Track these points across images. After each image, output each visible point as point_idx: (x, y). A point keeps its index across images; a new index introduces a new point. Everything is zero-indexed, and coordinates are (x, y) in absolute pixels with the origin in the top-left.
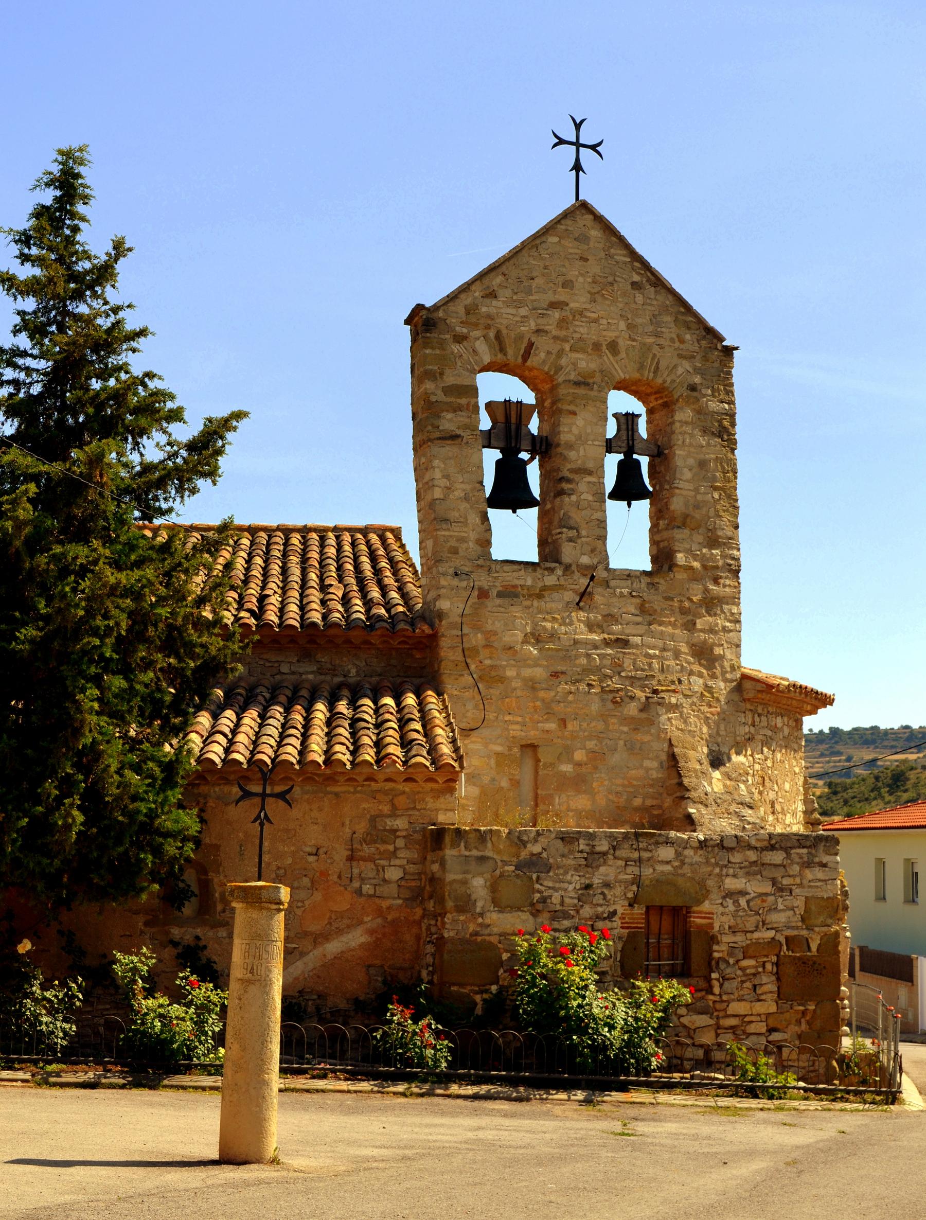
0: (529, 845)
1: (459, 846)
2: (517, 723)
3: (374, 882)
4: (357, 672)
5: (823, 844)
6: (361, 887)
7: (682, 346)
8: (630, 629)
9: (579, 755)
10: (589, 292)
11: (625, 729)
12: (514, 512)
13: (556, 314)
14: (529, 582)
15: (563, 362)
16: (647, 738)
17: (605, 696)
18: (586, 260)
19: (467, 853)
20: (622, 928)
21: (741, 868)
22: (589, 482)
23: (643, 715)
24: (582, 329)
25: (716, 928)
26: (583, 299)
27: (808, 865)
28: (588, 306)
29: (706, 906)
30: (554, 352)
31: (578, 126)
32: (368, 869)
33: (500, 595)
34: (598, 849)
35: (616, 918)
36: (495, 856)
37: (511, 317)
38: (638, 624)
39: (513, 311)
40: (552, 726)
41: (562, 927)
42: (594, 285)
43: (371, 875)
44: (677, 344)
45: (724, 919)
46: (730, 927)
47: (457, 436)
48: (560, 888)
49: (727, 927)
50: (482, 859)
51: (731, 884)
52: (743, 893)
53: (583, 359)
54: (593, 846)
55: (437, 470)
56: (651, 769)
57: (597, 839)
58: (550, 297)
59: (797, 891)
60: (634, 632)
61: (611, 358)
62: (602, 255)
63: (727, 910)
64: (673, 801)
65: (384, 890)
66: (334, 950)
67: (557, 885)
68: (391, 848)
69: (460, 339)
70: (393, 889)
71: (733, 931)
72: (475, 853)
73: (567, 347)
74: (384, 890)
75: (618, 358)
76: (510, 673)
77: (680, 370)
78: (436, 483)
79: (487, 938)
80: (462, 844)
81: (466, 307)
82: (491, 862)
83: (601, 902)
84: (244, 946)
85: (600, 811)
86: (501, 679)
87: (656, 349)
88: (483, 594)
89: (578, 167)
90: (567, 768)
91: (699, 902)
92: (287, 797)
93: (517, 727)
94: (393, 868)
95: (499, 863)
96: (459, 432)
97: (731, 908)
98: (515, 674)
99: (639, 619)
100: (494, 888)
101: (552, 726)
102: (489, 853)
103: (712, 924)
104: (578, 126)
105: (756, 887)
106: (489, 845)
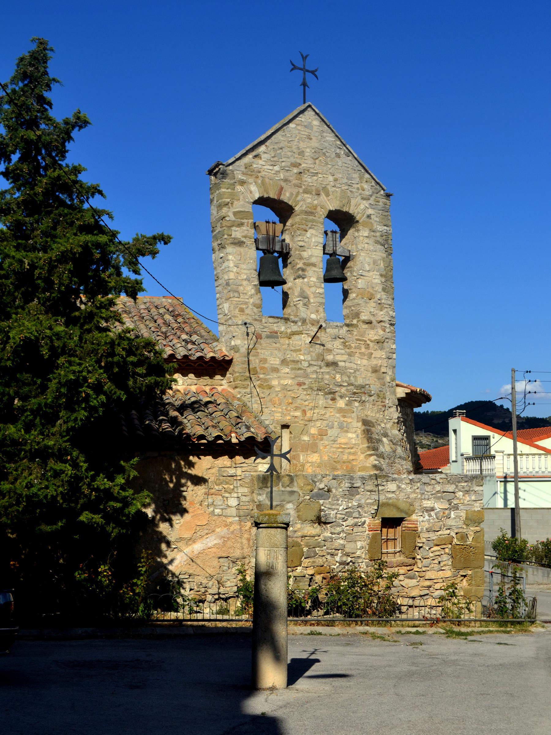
0: (317, 484)
1: (279, 485)
2: (279, 412)
3: (222, 507)
4: (183, 383)
5: (475, 480)
6: (214, 510)
7: (363, 192)
8: (338, 358)
9: (313, 431)
10: (313, 158)
11: (338, 415)
12: (273, 288)
13: (295, 170)
14: (283, 329)
15: (299, 198)
16: (349, 420)
17: (327, 396)
18: (311, 139)
19: (283, 489)
20: (369, 531)
21: (432, 495)
22: (314, 271)
23: (347, 407)
24: (308, 179)
25: (419, 529)
26: (310, 162)
27: (467, 492)
28: (312, 166)
29: (414, 517)
30: (294, 193)
31: (304, 58)
32: (218, 500)
33: (268, 337)
34: (355, 485)
35: (365, 526)
36: (299, 491)
37: (270, 171)
38: (342, 354)
39: (271, 168)
40: (298, 414)
41: (336, 531)
42: (315, 154)
43: (220, 503)
44: (360, 191)
45: (423, 524)
46: (426, 529)
47: (243, 242)
48: (334, 509)
49: (425, 529)
50: (292, 493)
51: (428, 504)
52: (433, 509)
53: (308, 198)
54: (353, 484)
55: (231, 262)
56: (352, 438)
57: (355, 479)
58: (292, 160)
59: (461, 507)
60: (341, 359)
61: (325, 198)
62: (320, 137)
63: (425, 519)
64: (365, 457)
65: (229, 512)
66: (199, 549)
67: (333, 507)
68: (232, 487)
69: (242, 183)
70: (233, 511)
71: (428, 531)
72: (288, 489)
73: (301, 191)
74: (229, 512)
75: (330, 197)
76: (275, 383)
77: (362, 207)
78: (231, 269)
79: (295, 539)
80: (280, 484)
81: (245, 164)
82: (296, 494)
83: (357, 516)
84: (266, 551)
85: (325, 463)
86: (270, 387)
87: (349, 194)
88: (259, 337)
89: (304, 85)
90: (306, 438)
91: (410, 515)
92: (288, 456)
93: (279, 415)
94: (233, 499)
95: (301, 495)
96: (243, 239)
97: (427, 517)
98: (277, 383)
99: (343, 352)
100: (298, 510)
101: (298, 414)
102: (295, 489)
103: (417, 527)
104: (304, 58)
105: (439, 506)
106: (295, 484)
